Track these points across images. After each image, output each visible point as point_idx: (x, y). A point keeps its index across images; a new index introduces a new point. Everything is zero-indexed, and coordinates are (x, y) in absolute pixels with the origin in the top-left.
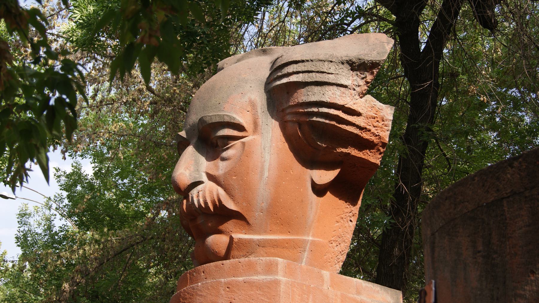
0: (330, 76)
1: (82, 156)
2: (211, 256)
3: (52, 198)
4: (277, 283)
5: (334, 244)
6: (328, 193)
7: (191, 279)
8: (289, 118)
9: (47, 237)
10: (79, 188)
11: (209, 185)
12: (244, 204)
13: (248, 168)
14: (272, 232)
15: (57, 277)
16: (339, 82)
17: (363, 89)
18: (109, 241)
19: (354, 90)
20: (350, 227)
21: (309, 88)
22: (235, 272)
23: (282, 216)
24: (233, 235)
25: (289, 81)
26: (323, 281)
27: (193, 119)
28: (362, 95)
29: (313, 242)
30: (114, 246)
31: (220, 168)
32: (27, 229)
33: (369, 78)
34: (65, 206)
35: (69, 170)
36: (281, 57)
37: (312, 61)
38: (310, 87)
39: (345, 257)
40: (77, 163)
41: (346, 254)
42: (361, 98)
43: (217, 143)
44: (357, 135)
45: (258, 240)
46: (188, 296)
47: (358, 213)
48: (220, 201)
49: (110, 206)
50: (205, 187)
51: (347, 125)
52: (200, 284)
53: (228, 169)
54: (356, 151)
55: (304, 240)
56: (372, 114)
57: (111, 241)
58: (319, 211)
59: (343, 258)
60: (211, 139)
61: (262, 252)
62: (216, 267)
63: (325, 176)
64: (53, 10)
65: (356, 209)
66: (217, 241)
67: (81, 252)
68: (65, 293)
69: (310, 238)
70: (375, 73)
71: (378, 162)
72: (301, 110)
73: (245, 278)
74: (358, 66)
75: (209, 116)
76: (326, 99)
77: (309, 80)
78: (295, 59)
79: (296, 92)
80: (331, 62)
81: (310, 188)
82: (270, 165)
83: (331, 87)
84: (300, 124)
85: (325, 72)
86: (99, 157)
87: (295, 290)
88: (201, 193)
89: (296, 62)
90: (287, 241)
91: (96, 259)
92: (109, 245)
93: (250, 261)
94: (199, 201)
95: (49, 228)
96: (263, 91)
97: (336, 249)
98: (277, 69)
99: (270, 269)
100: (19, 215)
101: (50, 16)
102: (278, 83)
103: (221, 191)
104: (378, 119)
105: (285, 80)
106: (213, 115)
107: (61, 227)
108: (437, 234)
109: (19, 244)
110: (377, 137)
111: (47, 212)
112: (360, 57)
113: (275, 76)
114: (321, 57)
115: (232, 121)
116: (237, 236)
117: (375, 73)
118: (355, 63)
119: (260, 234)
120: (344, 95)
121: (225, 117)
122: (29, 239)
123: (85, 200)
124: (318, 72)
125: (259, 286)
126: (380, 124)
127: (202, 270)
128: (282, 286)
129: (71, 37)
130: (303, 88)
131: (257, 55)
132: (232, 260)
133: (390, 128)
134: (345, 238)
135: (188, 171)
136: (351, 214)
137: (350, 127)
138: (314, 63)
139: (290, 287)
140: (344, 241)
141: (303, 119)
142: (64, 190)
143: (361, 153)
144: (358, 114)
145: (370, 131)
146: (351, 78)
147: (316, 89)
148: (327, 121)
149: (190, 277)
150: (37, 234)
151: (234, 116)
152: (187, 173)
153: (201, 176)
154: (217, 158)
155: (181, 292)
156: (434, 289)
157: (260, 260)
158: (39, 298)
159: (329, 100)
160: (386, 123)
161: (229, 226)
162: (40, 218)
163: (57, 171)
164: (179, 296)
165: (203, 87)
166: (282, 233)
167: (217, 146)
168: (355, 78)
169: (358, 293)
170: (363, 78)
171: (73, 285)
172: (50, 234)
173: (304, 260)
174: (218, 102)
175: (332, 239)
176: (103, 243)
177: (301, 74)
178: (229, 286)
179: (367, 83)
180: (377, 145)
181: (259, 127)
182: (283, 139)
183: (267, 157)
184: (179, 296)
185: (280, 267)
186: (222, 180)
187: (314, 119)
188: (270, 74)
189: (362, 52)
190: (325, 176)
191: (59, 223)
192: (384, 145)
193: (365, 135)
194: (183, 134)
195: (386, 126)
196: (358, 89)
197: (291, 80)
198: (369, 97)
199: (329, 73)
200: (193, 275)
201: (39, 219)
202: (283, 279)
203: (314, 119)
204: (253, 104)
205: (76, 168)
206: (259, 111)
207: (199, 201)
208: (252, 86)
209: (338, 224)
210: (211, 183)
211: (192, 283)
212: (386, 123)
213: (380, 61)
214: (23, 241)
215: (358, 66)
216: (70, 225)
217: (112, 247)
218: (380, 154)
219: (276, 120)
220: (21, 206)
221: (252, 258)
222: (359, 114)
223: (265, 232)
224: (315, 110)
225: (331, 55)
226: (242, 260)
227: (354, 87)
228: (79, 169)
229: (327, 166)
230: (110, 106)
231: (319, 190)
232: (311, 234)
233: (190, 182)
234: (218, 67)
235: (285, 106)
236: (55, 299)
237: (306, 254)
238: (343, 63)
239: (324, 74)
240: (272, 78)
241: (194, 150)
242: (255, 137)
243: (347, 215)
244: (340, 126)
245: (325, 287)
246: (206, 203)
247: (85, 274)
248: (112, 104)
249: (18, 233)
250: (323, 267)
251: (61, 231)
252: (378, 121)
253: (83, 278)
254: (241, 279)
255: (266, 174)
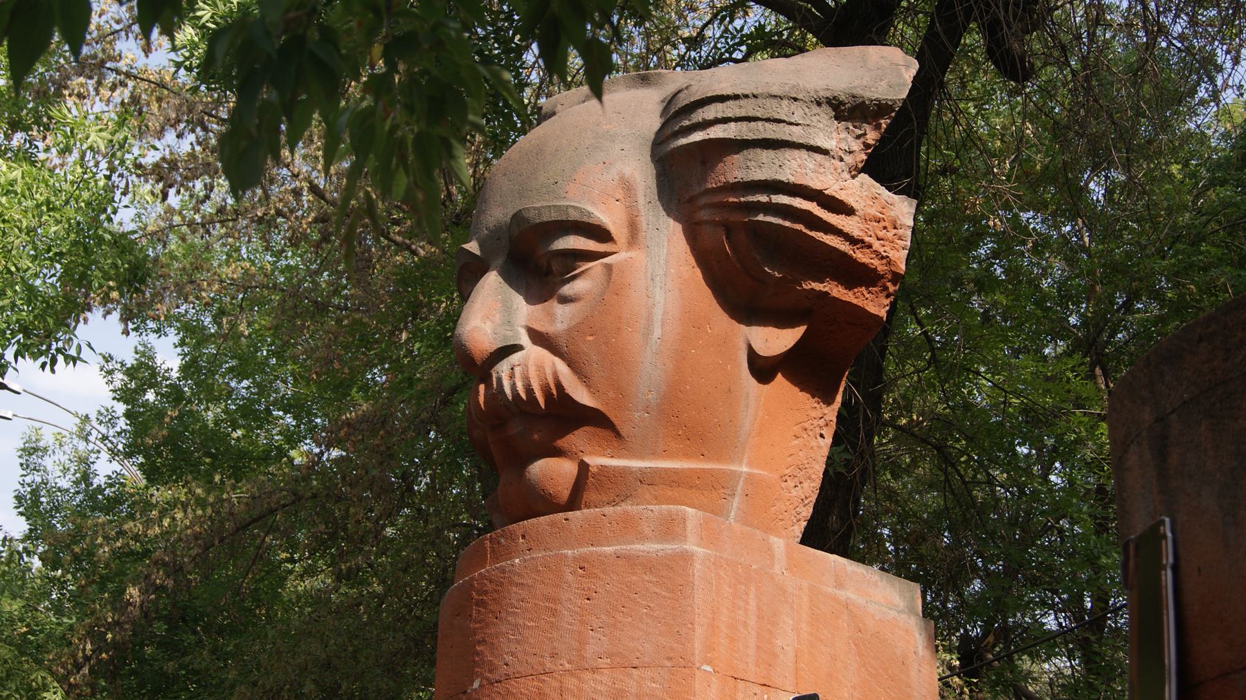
0: (794, 128)
1: (158, 331)
2: (541, 503)
3: (93, 416)
4: (686, 558)
5: (791, 484)
6: (779, 375)
7: (493, 551)
8: (704, 215)
9: (81, 497)
10: (150, 396)
11: (533, 354)
12: (611, 394)
13: (620, 318)
14: (667, 454)
15: (109, 580)
16: (812, 143)
17: (859, 159)
18: (224, 500)
19: (841, 160)
20: (820, 447)
21: (751, 153)
22: (594, 535)
23: (690, 421)
24: (587, 459)
25: (707, 137)
26: (772, 557)
27: (497, 213)
28: (855, 171)
29: (750, 477)
30: (236, 510)
31: (559, 317)
32: (38, 479)
33: (872, 136)
34: (119, 434)
35: (130, 361)
36: (687, 88)
37: (755, 96)
38: (751, 151)
39: (811, 510)
40: (145, 346)
41: (812, 505)
42: (853, 177)
43: (549, 266)
44: (844, 254)
45: (640, 469)
46: (489, 587)
47: (835, 420)
48: (559, 386)
49: (213, 438)
50: (527, 358)
51: (826, 234)
52: (517, 561)
53: (577, 320)
54: (840, 288)
55: (732, 471)
56: (873, 211)
57: (229, 500)
58: (760, 413)
59: (807, 512)
60: (539, 257)
61: (648, 496)
62: (553, 524)
63: (777, 340)
64: (118, 22)
65: (831, 412)
66: (552, 472)
67: (166, 522)
68: (130, 608)
69: (745, 469)
70: (884, 126)
71: (883, 313)
72: (731, 200)
73: (618, 547)
74: (848, 110)
75: (535, 208)
76: (786, 176)
77: (751, 136)
78: (719, 93)
79: (721, 161)
80: (795, 99)
81: (745, 365)
82: (665, 313)
83: (796, 153)
84: (729, 229)
85: (784, 121)
86: (192, 334)
87: (722, 573)
88: (518, 370)
89: (722, 99)
90: (699, 474)
91: (196, 537)
92: (225, 511)
93: (626, 513)
94: (513, 386)
95: (86, 477)
96: (649, 158)
97: (794, 493)
98: (678, 114)
99: (670, 528)
100: (23, 450)
101: (112, 33)
102: (683, 141)
103: (562, 367)
104: (887, 224)
105: (698, 136)
106: (542, 206)
107: (109, 477)
108: (1174, 416)
109: (21, 509)
110: (884, 261)
111: (82, 446)
112: (855, 92)
113: (676, 128)
114: (775, 90)
115: (585, 219)
116: (595, 461)
117: (884, 126)
118: (844, 104)
119: (641, 457)
120: (822, 170)
121: (571, 211)
122: (43, 499)
123: (167, 420)
124: (768, 120)
125: (649, 565)
126: (890, 235)
127: (519, 533)
128: (697, 566)
129: (187, 59)
130: (737, 153)
131: (628, 87)
132: (585, 511)
133: (909, 243)
134: (811, 472)
135: (489, 323)
136: (822, 422)
137: (832, 237)
138: (760, 101)
139: (713, 567)
140: (810, 478)
141: (736, 217)
142: (118, 400)
143: (850, 293)
144: (848, 211)
145: (870, 246)
146: (834, 134)
147: (765, 155)
148: (787, 224)
149: (492, 548)
150: (60, 490)
151: (590, 208)
152: (488, 327)
153: (517, 334)
154: (551, 297)
155: (472, 579)
156: (1169, 535)
157: (649, 510)
158: (65, 620)
159: (792, 179)
160: (901, 232)
161: (578, 439)
162: (67, 457)
163: (107, 361)
164: (469, 586)
165: (511, 153)
166: (687, 456)
167: (549, 272)
168: (844, 135)
169: (840, 585)
170: (858, 137)
171: (147, 591)
172: (86, 491)
173: (733, 513)
174: (552, 181)
175: (787, 472)
176: (211, 504)
177: (733, 124)
178: (583, 565)
179: (867, 146)
180: (882, 277)
181: (641, 235)
182: (692, 261)
183: (659, 296)
184: (469, 586)
185: (690, 525)
186: (562, 342)
187: (761, 217)
188: (663, 126)
189: (857, 83)
190: (777, 340)
191: (104, 468)
192: (896, 278)
193: (861, 256)
194: (473, 247)
195: (900, 239)
196: (849, 159)
197: (712, 136)
198: (864, 177)
199: (791, 124)
200: (499, 543)
201: (64, 458)
202: (700, 550)
203: (761, 217)
204: (627, 186)
205: (143, 354)
206: (641, 200)
207: (513, 386)
208: (626, 147)
209: (796, 442)
210: (540, 349)
211: (496, 559)
212: (901, 232)
213: (894, 101)
214: (29, 504)
215: (848, 110)
216: (132, 472)
217: (232, 514)
218: (887, 297)
219: (676, 219)
220: (28, 432)
221: (627, 507)
222: (848, 211)
223: (654, 454)
224: (763, 198)
225: (794, 86)
226: (608, 510)
227: (841, 153)
228: (152, 358)
229: (781, 320)
230: (231, 224)
231: (763, 369)
232: (745, 460)
233: (495, 347)
234: (543, 112)
235: (697, 190)
236: (110, 620)
237: (736, 502)
238: (819, 104)
239: (782, 125)
240: (669, 131)
241: (501, 280)
242: (633, 254)
243: (816, 422)
244: (813, 234)
245: (777, 569)
246: (529, 390)
247: (176, 570)
248: (234, 220)
249: (20, 487)
250: (768, 530)
251: (111, 485)
252: (885, 228)
253: (168, 576)
254: (609, 549)
255: (657, 332)
